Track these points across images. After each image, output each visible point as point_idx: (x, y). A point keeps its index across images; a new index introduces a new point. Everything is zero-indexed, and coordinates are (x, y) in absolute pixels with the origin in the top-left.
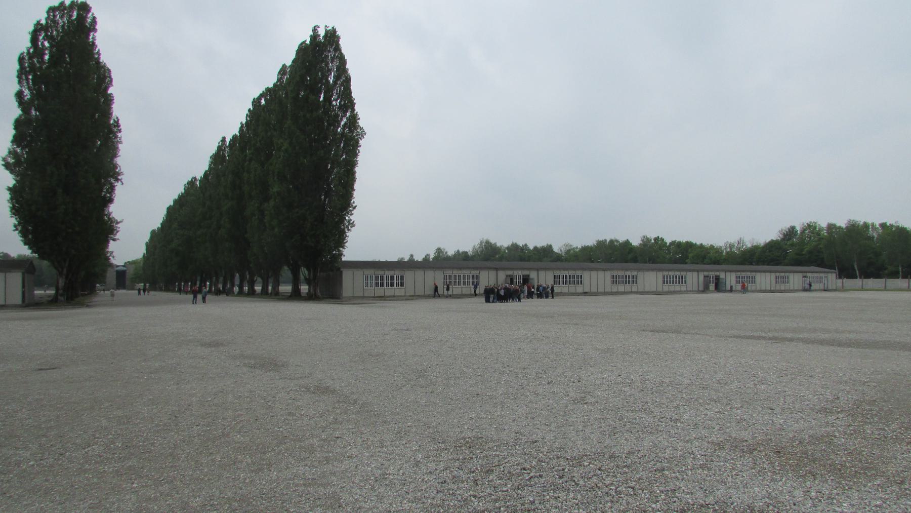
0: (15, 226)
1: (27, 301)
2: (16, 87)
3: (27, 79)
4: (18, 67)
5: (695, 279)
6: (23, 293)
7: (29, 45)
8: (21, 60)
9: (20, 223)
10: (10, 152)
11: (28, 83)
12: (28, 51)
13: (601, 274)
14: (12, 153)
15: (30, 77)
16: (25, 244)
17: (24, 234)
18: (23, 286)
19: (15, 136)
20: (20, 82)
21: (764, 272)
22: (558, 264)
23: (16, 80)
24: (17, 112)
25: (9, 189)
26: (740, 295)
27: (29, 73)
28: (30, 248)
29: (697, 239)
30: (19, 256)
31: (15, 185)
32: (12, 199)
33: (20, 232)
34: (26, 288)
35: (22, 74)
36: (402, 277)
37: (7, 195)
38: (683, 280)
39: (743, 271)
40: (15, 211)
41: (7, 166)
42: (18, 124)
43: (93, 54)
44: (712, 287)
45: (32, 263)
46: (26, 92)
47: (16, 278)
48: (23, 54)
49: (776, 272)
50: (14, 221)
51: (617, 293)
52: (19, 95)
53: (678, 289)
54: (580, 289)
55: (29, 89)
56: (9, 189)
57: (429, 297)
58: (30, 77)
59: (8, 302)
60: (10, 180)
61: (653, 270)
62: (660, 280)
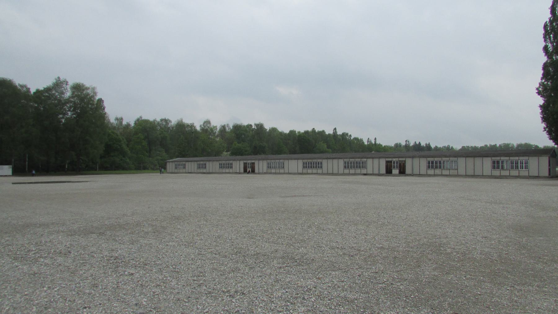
0: (544, 128)
1: (551, 175)
2: (543, 44)
3: (550, 37)
4: (543, 32)
5: (238, 166)
6: (549, 170)
7: (550, 16)
8: (545, 26)
9: (547, 127)
10: (540, 84)
11: (550, 39)
12: (550, 19)
13: (335, 161)
14: (541, 84)
15: (551, 36)
16: (550, 139)
17: (550, 133)
18: (549, 165)
19: (543, 74)
20: (545, 41)
21: (191, 161)
22: (422, 153)
23: (543, 40)
24: (544, 59)
25: (541, 106)
26: (381, 179)
27: (551, 33)
28: (554, 142)
29: (355, 133)
30: (545, 147)
31: (544, 104)
32: (542, 112)
33: (548, 132)
34: (551, 165)
35: (546, 36)
36: (321, 163)
37: (539, 110)
38: (364, 166)
39: (315, 159)
40: (544, 119)
41: (539, 93)
42: (545, 67)
43: (20, 90)
44: (395, 171)
45: (554, 151)
46: (550, 45)
47: (545, 160)
48: (546, 22)
49: (197, 161)
50: (543, 125)
51: (223, 173)
52: (545, 49)
53: (278, 171)
54: (364, 171)
55: (551, 43)
56: (541, 106)
57: (545, 178)
58: (551, 36)
59: (540, 175)
60: (541, 101)
61: (295, 159)
62: (218, 166)
